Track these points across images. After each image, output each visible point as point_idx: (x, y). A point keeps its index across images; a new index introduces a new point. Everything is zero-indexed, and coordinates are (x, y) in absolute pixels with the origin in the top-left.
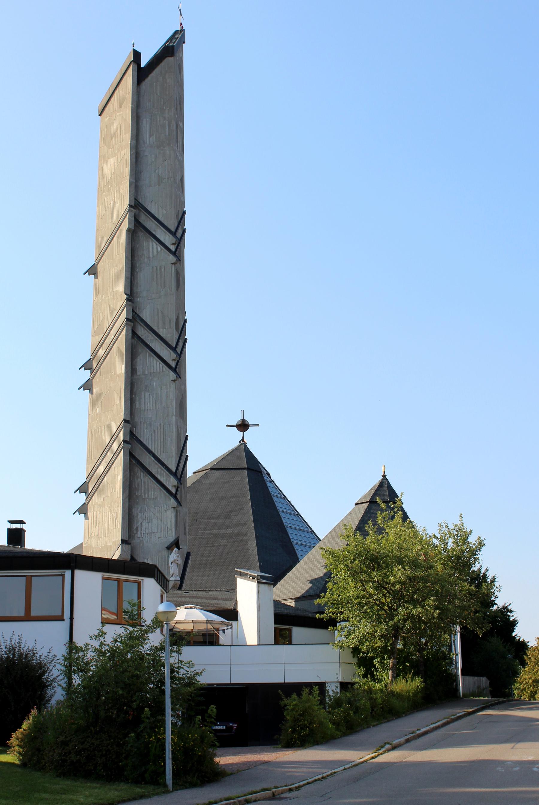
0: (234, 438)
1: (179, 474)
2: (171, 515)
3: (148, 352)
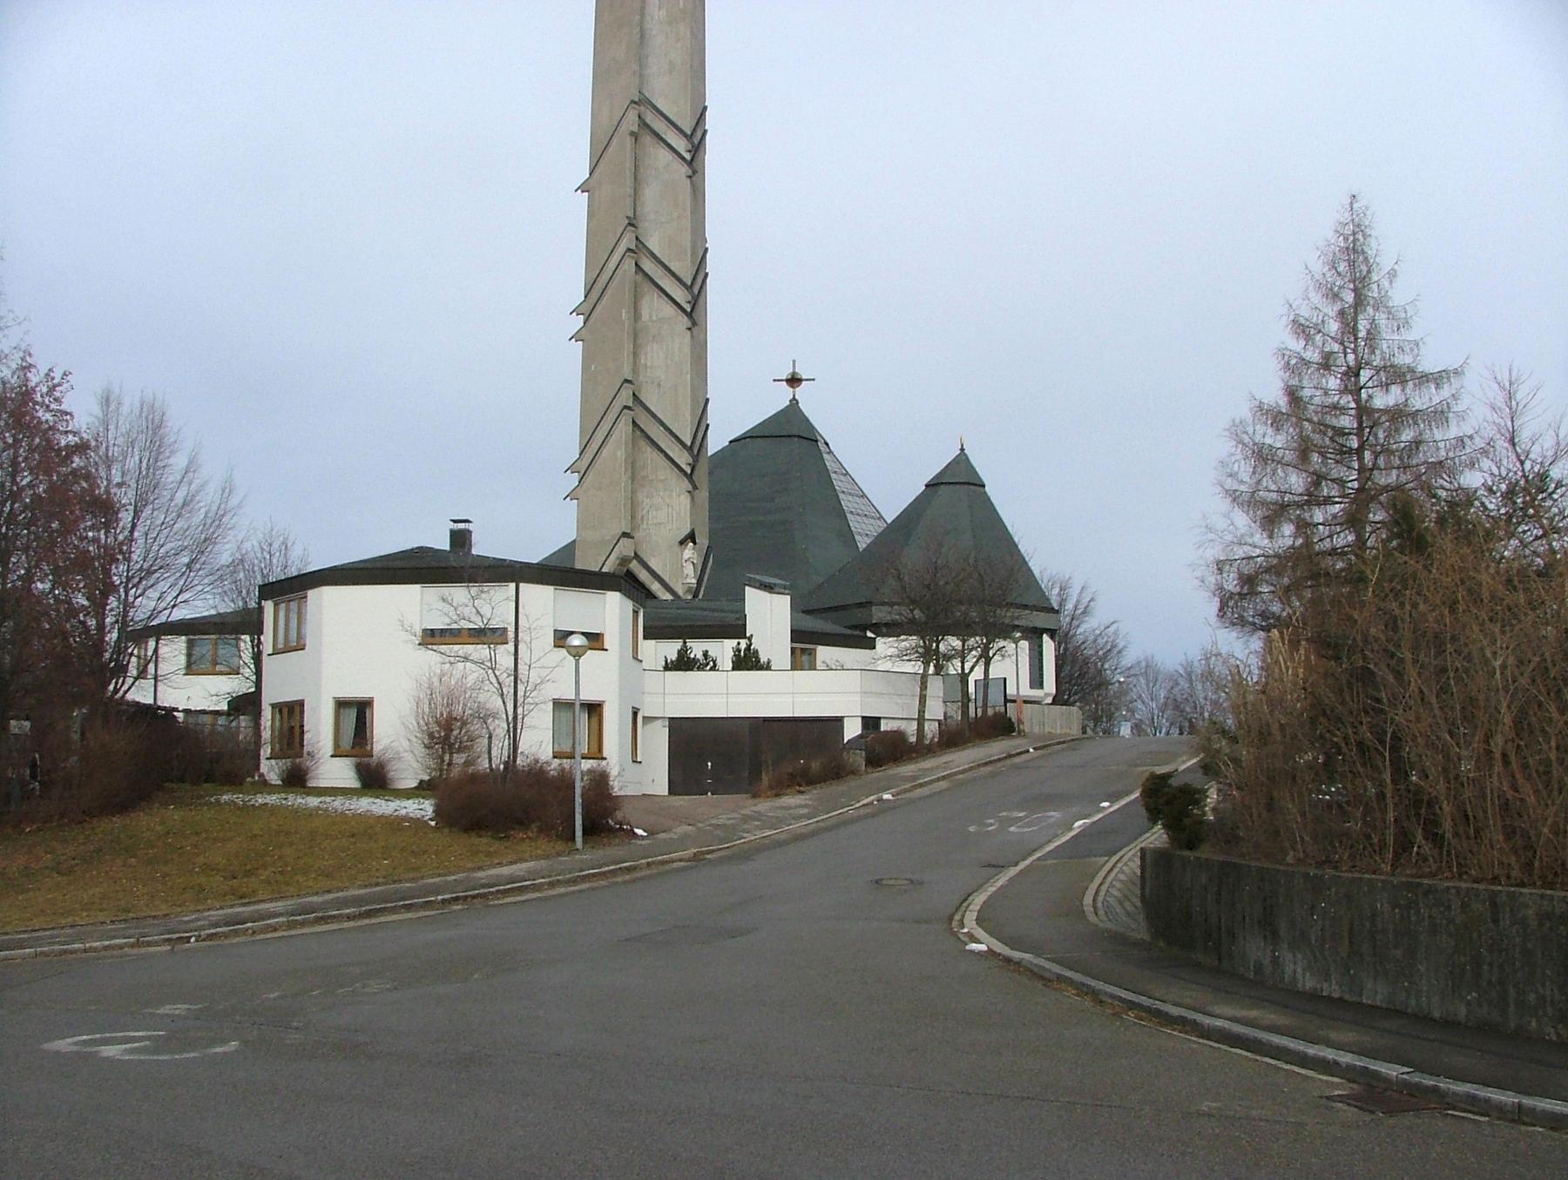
0: (780, 398)
1: (696, 447)
2: (685, 500)
3: (656, 293)
